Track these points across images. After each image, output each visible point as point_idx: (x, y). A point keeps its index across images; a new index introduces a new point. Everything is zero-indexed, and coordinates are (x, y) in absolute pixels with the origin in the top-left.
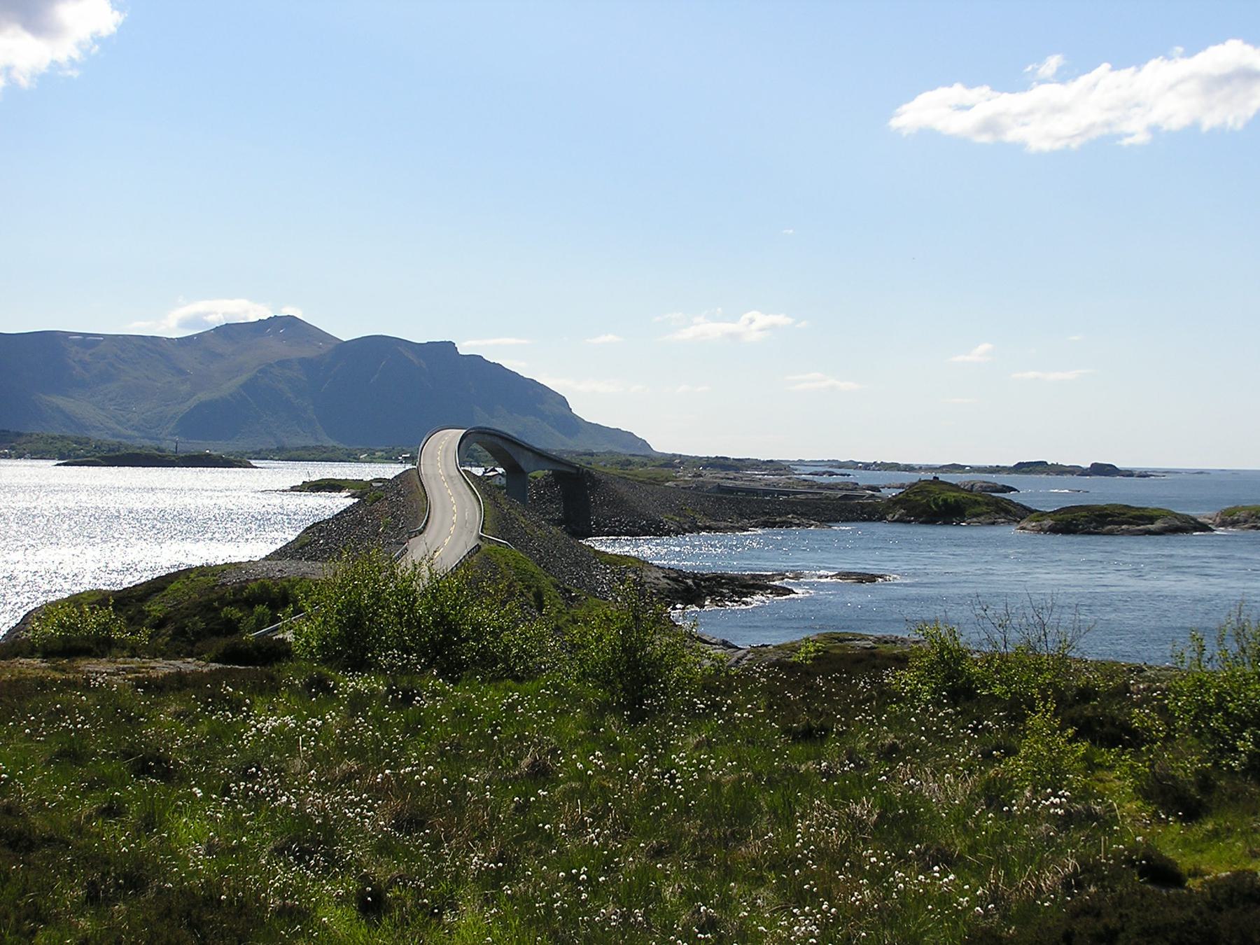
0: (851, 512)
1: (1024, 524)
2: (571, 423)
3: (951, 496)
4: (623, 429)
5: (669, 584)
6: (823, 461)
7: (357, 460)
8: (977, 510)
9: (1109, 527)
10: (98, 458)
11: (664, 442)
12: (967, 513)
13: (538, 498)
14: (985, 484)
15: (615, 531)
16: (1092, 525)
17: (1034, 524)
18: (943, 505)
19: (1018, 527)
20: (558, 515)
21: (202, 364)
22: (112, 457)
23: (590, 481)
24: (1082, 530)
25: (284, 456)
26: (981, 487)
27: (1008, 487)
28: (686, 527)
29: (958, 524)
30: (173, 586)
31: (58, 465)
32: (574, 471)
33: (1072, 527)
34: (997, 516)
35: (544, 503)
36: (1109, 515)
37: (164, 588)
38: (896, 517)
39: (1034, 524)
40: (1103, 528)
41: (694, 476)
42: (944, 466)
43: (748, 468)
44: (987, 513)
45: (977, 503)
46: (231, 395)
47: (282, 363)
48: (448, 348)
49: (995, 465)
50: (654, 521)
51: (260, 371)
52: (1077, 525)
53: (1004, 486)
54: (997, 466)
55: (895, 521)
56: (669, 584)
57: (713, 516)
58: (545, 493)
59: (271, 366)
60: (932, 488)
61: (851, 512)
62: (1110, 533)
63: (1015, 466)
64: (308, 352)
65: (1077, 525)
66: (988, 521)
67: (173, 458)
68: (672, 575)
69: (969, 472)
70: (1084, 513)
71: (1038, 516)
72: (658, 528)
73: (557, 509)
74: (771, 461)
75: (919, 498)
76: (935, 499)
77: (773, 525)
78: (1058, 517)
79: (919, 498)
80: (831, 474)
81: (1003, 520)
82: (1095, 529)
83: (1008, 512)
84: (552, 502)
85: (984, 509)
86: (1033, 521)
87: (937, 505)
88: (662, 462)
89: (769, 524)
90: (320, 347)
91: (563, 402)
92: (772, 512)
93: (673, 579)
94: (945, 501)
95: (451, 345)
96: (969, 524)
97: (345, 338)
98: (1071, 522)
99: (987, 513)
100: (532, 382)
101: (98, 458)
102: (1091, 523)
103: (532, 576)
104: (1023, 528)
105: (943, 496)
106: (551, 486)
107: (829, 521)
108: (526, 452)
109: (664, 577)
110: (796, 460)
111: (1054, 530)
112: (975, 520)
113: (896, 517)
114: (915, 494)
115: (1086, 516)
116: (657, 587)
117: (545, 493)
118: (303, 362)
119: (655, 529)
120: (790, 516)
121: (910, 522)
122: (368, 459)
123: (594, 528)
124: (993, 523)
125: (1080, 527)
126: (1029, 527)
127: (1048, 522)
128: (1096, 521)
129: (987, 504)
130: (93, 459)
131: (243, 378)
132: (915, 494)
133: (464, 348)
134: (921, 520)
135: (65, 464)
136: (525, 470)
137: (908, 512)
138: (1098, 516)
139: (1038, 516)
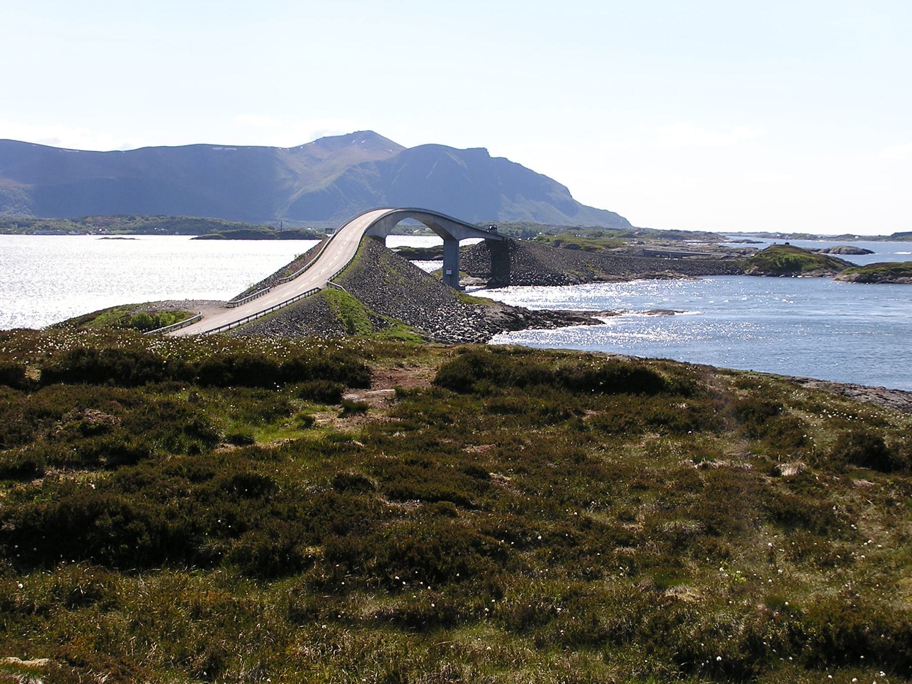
0: (718, 268)
1: (838, 276)
2: (571, 206)
3: (792, 256)
4: (609, 210)
5: (502, 317)
6: (756, 233)
7: (411, 234)
8: (811, 266)
9: (902, 278)
10: (220, 234)
11: (638, 221)
12: (803, 269)
13: (474, 259)
14: (849, 248)
15: (527, 281)
16: (888, 277)
17: (845, 276)
18: (785, 263)
19: (834, 279)
20: (487, 271)
21: (306, 166)
22: (230, 233)
23: (512, 246)
24: (879, 280)
25: (139, 222)
26: (846, 250)
27: (867, 250)
28: (583, 279)
29: (796, 277)
30: (99, 318)
31: (193, 239)
32: (500, 239)
33: (873, 279)
34: (826, 271)
35: (478, 262)
36: (903, 270)
37: (94, 319)
38: (751, 271)
39: (845, 276)
40: (897, 279)
41: (638, 244)
42: (840, 236)
43: (690, 238)
44: (818, 268)
45: (811, 261)
46: (326, 188)
47: (363, 165)
48: (482, 152)
49: (877, 235)
50: (557, 275)
51: (347, 171)
52: (876, 277)
53: (863, 250)
54: (879, 236)
55: (751, 275)
56: (502, 317)
57: (607, 272)
58: (479, 255)
59: (355, 166)
60: (780, 250)
61: (718, 268)
62: (901, 283)
63: (892, 235)
64: (382, 157)
65: (876, 277)
66: (818, 274)
67: (273, 234)
68: (508, 311)
69: (857, 240)
70: (883, 268)
71: (849, 271)
72: (560, 279)
73: (487, 266)
74: (711, 233)
75: (769, 258)
76: (780, 258)
77: (653, 277)
78: (864, 271)
79: (769, 258)
80: (749, 242)
81: (829, 273)
82: (890, 279)
83: (834, 268)
84: (483, 261)
85: (816, 265)
86: (845, 274)
87: (781, 263)
88: (625, 234)
89: (650, 277)
90: (390, 153)
91: (566, 191)
92: (657, 268)
93: (510, 314)
94: (787, 260)
95: (484, 151)
96: (804, 276)
97: (408, 147)
98: (872, 274)
99: (818, 268)
100: (544, 177)
101: (220, 234)
102: (887, 275)
103: (352, 310)
104: (838, 280)
105: (785, 257)
106: (484, 250)
107: (701, 275)
108: (456, 225)
109: (501, 312)
110: (737, 232)
111: (859, 280)
112: (808, 273)
113: (751, 271)
114: (767, 255)
115: (884, 271)
116: (493, 319)
117: (479, 255)
118: (378, 163)
119: (557, 280)
120: (667, 271)
121: (761, 275)
122: (420, 233)
123: (512, 280)
124: (822, 276)
125: (879, 278)
126: (842, 278)
127: (855, 275)
128: (892, 274)
129: (819, 262)
130: (216, 234)
131: (334, 177)
132: (767, 255)
133: (493, 154)
134: (768, 274)
135: (197, 239)
136: (456, 238)
137: (760, 268)
138: (892, 270)
139: (849, 271)
